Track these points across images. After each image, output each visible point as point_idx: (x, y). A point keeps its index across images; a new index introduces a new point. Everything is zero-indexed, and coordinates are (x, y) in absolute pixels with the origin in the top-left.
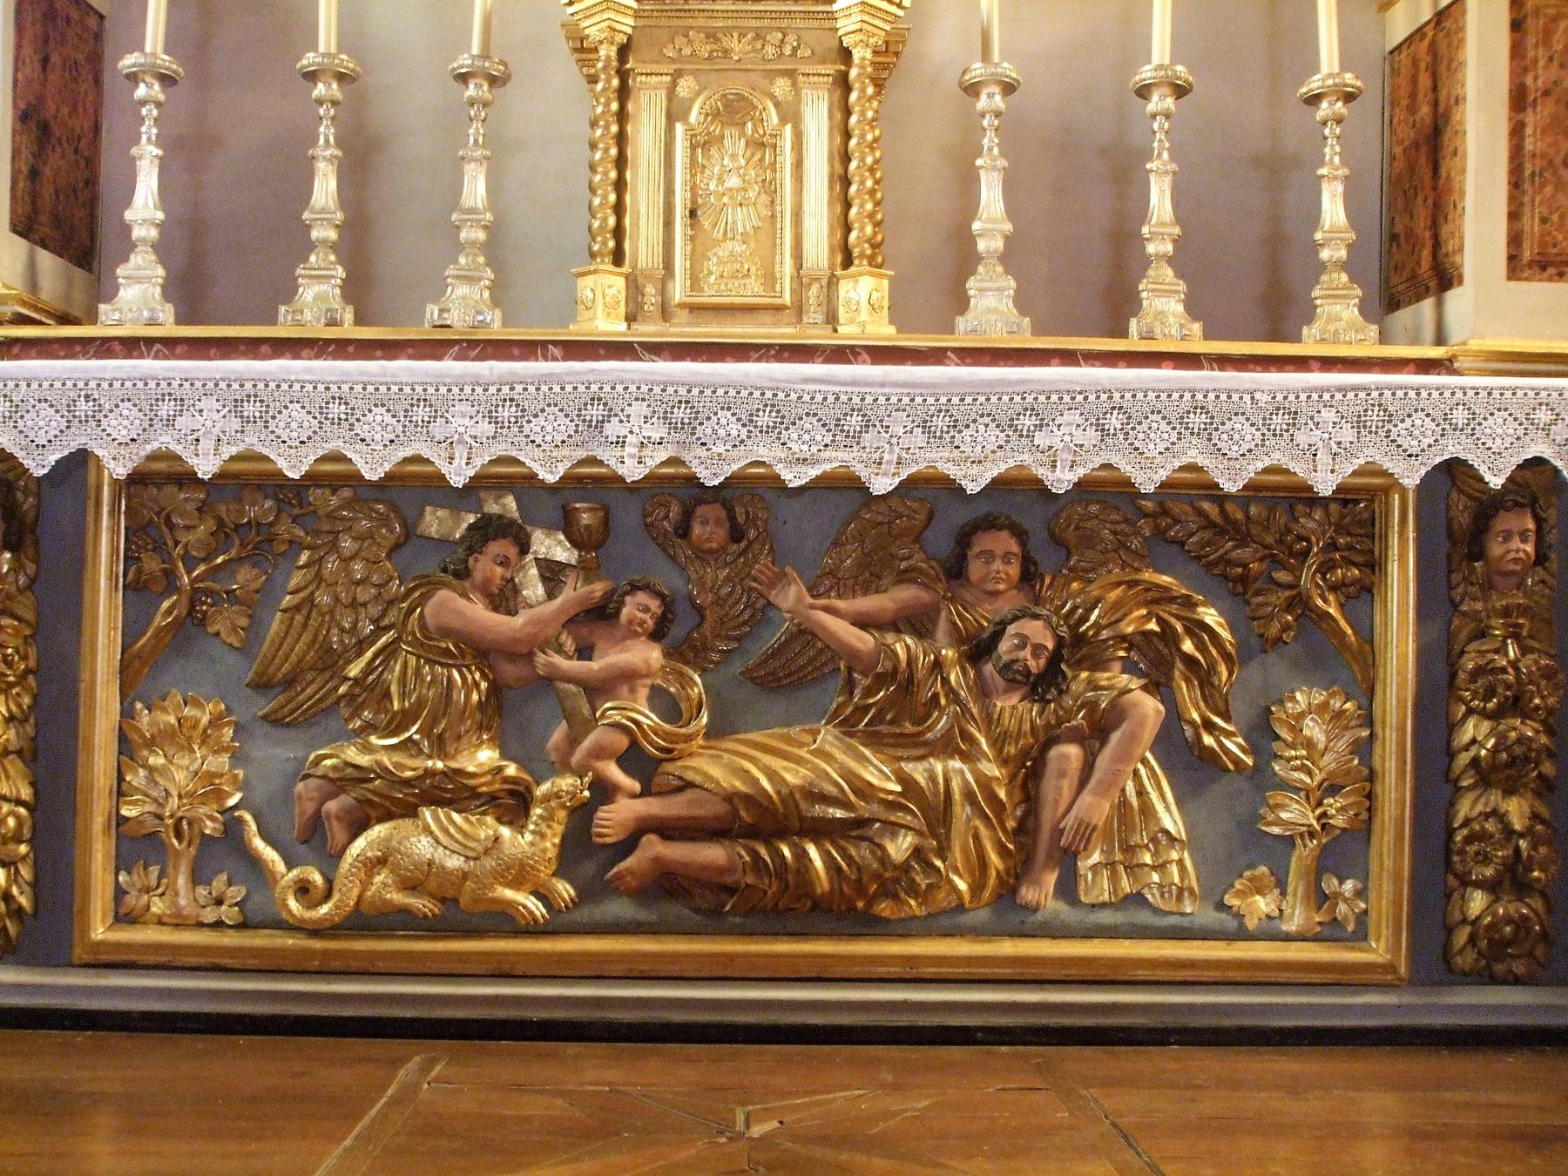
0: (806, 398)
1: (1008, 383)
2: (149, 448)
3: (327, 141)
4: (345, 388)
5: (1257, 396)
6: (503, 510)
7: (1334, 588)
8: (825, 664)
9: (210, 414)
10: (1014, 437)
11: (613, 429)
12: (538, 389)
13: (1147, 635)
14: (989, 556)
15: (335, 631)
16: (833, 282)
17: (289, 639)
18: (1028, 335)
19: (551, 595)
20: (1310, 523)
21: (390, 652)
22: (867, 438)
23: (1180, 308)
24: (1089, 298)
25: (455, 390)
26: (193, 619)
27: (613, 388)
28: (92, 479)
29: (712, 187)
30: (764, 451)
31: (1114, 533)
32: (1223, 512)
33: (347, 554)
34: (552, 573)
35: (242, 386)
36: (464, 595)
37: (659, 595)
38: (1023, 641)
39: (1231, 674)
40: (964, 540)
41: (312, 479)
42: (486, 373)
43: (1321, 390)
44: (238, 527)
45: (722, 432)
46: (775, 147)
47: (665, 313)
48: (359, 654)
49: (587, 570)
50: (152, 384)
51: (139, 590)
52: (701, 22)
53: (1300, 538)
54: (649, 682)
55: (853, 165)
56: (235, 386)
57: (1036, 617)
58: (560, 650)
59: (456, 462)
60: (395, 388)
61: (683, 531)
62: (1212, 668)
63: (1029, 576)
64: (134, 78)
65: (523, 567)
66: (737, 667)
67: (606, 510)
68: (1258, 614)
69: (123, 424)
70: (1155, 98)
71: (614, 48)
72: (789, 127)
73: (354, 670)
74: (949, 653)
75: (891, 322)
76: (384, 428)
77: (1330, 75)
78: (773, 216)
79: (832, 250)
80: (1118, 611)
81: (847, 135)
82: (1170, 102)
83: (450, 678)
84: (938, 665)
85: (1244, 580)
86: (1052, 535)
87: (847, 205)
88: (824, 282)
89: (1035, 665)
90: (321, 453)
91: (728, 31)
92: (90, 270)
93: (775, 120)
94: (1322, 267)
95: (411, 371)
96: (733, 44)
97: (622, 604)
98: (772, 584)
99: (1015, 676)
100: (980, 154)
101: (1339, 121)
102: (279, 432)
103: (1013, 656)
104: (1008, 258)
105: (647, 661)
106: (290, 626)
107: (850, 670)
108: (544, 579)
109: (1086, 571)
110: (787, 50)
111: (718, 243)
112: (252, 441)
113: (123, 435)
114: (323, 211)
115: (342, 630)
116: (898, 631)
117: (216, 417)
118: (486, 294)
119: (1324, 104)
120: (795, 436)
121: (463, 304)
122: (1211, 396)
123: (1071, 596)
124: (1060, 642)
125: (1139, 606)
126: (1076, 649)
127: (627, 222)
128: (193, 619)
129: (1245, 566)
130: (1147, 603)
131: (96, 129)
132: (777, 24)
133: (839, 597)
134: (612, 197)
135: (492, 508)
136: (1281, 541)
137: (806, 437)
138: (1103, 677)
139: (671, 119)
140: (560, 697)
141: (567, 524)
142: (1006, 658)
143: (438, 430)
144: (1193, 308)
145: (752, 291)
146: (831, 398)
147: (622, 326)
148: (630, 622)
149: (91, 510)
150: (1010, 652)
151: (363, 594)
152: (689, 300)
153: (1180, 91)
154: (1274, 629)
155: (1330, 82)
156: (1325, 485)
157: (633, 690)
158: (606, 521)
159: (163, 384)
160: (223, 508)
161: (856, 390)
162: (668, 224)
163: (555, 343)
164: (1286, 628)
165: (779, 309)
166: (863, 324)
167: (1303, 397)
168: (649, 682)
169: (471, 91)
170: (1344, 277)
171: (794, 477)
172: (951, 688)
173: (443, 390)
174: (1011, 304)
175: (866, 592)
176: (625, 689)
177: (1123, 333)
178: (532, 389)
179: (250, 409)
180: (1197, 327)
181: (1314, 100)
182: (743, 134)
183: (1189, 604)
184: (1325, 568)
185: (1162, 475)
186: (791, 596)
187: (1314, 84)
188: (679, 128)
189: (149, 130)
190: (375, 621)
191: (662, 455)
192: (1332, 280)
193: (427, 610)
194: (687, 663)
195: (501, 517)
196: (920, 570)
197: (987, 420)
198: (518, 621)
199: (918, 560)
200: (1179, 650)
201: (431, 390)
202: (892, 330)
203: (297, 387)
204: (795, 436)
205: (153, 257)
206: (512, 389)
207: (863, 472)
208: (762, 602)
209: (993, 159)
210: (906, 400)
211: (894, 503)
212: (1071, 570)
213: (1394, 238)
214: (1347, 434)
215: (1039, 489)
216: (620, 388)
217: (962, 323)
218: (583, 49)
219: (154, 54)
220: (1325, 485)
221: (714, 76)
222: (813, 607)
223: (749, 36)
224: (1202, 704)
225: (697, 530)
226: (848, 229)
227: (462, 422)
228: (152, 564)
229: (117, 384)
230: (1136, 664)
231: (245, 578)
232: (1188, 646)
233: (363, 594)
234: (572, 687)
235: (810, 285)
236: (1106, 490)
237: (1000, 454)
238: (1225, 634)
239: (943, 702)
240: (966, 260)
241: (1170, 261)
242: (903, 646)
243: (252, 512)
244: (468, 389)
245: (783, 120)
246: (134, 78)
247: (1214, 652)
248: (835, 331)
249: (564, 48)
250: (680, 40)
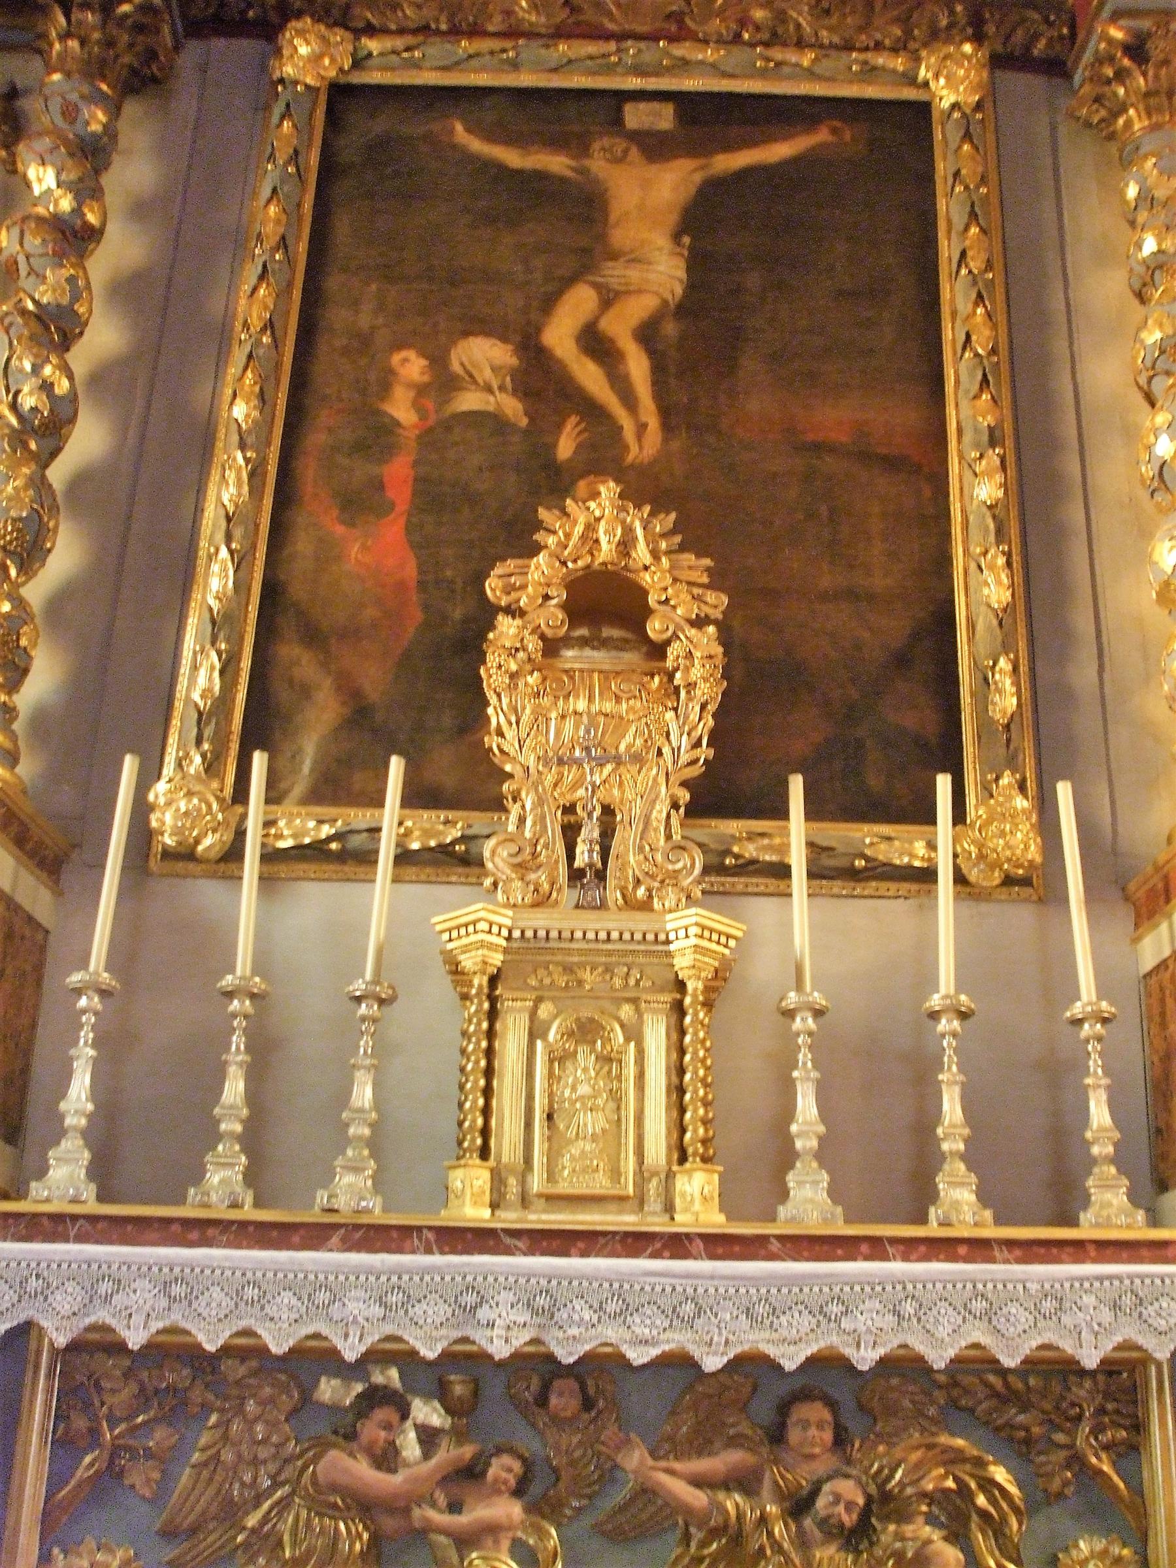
0: (648, 1288)
1: (817, 1276)
2: (88, 1321)
3: (238, 1048)
4: (259, 1274)
5: (1028, 1285)
6: (390, 1380)
7: (1106, 1447)
8: (667, 1518)
9: (139, 1292)
10: (824, 1322)
11: (484, 1314)
12: (422, 1279)
13: (946, 1491)
14: (805, 1424)
15: (237, 1486)
16: (670, 1176)
17: (196, 1492)
18: (841, 1222)
19: (426, 1456)
20: (1081, 1391)
21: (283, 1505)
22: (699, 1323)
23: (973, 1197)
24: (890, 1200)
25: (352, 1278)
26: (112, 1473)
27: (485, 1279)
28: (33, 1345)
29: (567, 1094)
30: (612, 1333)
31: (912, 1402)
32: (1006, 1384)
33: (250, 1417)
34: (428, 1437)
35: (171, 1270)
36: (352, 1455)
37: (521, 1457)
38: (837, 1498)
39: (1020, 1524)
40: (784, 1409)
41: (226, 1350)
42: (378, 1265)
43: (1081, 1280)
44: (157, 1391)
45: (576, 1317)
46: (620, 1062)
47: (525, 1201)
48: (257, 1506)
49: (459, 1435)
50: (95, 1266)
51: (65, 1445)
52: (559, 958)
53: (1073, 1405)
54: (510, 1534)
55: (688, 1077)
56: (166, 1270)
57: (847, 1476)
58: (434, 1505)
59: (350, 1340)
60: (301, 1276)
61: (542, 1400)
62: (1004, 1520)
63: (840, 1440)
64: (78, 992)
65: (403, 1432)
66: (587, 1521)
67: (476, 1382)
68: (1042, 1471)
69: (65, 1300)
70: (944, 1021)
71: (485, 979)
72: (632, 1044)
73: (252, 1521)
74: (772, 1509)
75: (721, 1210)
76: (291, 1309)
77: (1090, 1003)
78: (619, 1120)
79: (669, 1148)
80: (918, 1471)
81: (682, 1052)
82: (956, 1024)
83: (337, 1529)
84: (763, 1520)
85: (1028, 1442)
86: (859, 1402)
87: (682, 1110)
88: (663, 1176)
89: (849, 1520)
90: (234, 1329)
91: (582, 965)
92: (16, 1146)
93: (621, 1039)
94: (1094, 1161)
95: (314, 1261)
96: (587, 976)
97: (488, 1464)
98: (618, 1448)
99: (832, 1530)
100: (795, 1067)
101: (1099, 1039)
102: (200, 1310)
103: (830, 1511)
104: (821, 1156)
105: (509, 1516)
106: (196, 1482)
107: (687, 1525)
108: (421, 1441)
109: (890, 1435)
110: (632, 982)
111: (570, 1142)
112: (176, 1317)
113: (66, 1309)
114: (231, 1107)
115: (243, 1484)
116: (728, 1489)
117: (147, 1295)
118: (369, 1183)
119: (1086, 1026)
120: (638, 1320)
121: (351, 1190)
122: (990, 1286)
123: (881, 1457)
124: (869, 1499)
125: (937, 1465)
126: (883, 1504)
127: (493, 1123)
128: (112, 1473)
129: (1027, 1430)
130: (944, 1464)
131: (33, 1026)
132: (623, 960)
133: (676, 1458)
134: (482, 1082)
135: (378, 1378)
136: (1057, 1408)
137: (648, 1322)
138: (909, 1529)
139: (532, 1037)
140: (432, 1546)
141: (441, 1393)
142: (823, 1513)
143: (335, 1311)
144: (984, 1197)
145: (600, 1184)
146: (669, 1289)
147: (486, 1213)
148: (496, 1481)
149: (30, 1374)
150: (825, 1507)
151: (263, 1453)
152: (546, 1191)
153: (964, 1016)
154: (1056, 1484)
155: (1089, 1009)
156: (1090, 1360)
157: (497, 1542)
158: (476, 1393)
159: (104, 1267)
160: (146, 1374)
161: (690, 1282)
162: (529, 1125)
163: (430, 1228)
164: (1066, 1483)
165: (622, 1199)
166: (697, 1214)
167: (1067, 1285)
168: (510, 1534)
169: (363, 1009)
170: (1113, 1170)
171: (638, 1356)
172: (776, 1541)
173: (342, 1278)
174: (825, 1195)
175: (700, 1454)
176: (490, 1542)
177: (922, 1220)
178: (416, 1278)
179: (176, 1290)
180: (988, 1214)
181: (1078, 1022)
182: (593, 1050)
183: (980, 1463)
184: (1097, 1431)
185: (951, 1353)
186: (635, 1459)
187: (1077, 1009)
188: (539, 1043)
189: (86, 1035)
190: (273, 1477)
191: (526, 1336)
192: (1102, 1172)
193: (319, 1467)
194: (544, 1517)
195: (385, 1387)
196: (746, 1437)
197: (800, 1307)
198: (397, 1480)
199: (745, 1428)
200: (974, 1504)
201: (331, 1278)
202: (721, 1218)
203: (218, 1272)
204: (638, 1320)
205: (81, 1142)
206: (400, 1278)
207: (696, 1352)
208: (608, 1465)
209: (807, 1071)
210: (732, 1291)
211: (722, 1378)
212: (877, 1436)
213: (1159, 1131)
214: (1106, 1316)
215: (844, 1365)
216: (491, 1279)
217: (783, 1212)
218: (456, 972)
219: (97, 973)
220: (1090, 1360)
221: (569, 1002)
222: (653, 1468)
223: (600, 970)
224: (997, 1553)
225: (554, 1400)
226: (683, 1130)
227: (356, 1306)
228: (80, 1423)
229: (65, 1266)
230: (937, 1518)
231: (160, 1437)
232: (981, 1500)
233: (263, 1453)
234: (442, 1539)
235: (650, 1180)
236: (903, 1366)
237: (811, 1336)
238: (1013, 1490)
239: (769, 1552)
240: (785, 1157)
241: (963, 1157)
242: (733, 1502)
243: (170, 1377)
244: (362, 1278)
245: (628, 1040)
246: (78, 992)
247: (1004, 1505)
248: (673, 1219)
249: (440, 970)
250: (541, 972)
